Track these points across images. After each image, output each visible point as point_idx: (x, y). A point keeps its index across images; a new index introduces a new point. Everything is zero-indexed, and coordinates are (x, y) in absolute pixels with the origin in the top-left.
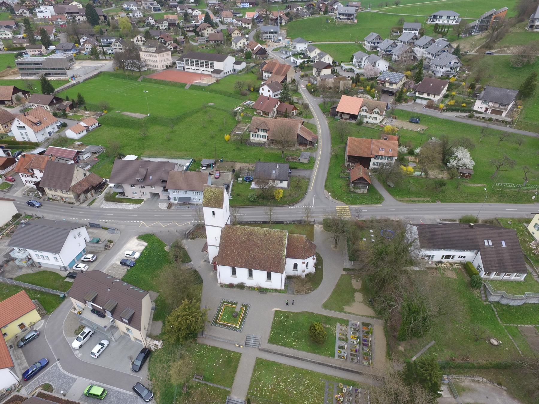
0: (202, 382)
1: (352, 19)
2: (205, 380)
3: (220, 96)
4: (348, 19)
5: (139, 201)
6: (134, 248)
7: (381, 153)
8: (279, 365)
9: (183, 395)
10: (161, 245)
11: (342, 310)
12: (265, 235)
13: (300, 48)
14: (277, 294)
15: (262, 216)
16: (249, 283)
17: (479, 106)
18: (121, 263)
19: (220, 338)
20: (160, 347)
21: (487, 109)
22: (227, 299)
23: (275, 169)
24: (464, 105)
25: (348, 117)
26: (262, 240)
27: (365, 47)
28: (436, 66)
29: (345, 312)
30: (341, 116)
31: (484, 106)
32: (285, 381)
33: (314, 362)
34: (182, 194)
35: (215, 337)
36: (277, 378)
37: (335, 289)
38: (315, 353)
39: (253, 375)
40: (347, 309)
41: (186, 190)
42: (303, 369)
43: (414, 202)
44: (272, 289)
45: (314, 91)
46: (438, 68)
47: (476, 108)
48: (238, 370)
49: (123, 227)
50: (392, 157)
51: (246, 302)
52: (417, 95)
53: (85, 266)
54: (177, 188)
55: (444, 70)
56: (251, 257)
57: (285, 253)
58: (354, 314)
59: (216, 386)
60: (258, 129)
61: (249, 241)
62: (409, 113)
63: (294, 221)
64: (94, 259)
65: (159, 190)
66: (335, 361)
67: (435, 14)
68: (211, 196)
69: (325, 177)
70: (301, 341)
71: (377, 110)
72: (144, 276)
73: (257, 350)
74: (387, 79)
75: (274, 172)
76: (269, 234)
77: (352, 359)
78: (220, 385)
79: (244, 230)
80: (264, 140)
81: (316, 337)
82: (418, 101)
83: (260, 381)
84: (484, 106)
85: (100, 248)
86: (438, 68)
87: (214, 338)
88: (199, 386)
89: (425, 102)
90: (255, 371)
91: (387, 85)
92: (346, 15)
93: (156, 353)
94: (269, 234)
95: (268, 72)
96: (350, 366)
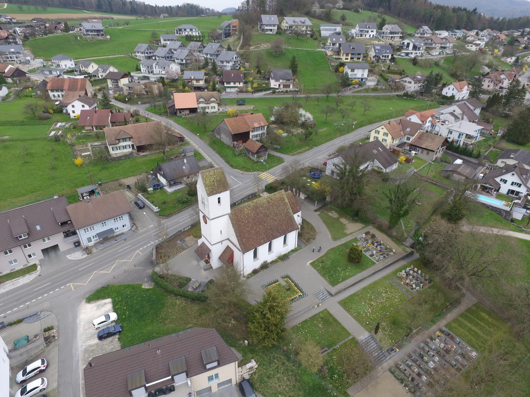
0: (329, 351)
1: (102, 35)
2: (329, 348)
3: (6, 127)
4: (98, 35)
5: (34, 267)
6: (99, 314)
7: (256, 125)
8: (355, 294)
9: (327, 375)
10: (135, 288)
11: (346, 235)
12: (269, 202)
13: (66, 65)
14: (297, 253)
15: (252, 187)
16: (270, 258)
17: (273, 84)
18: (101, 338)
19: (299, 312)
20: (257, 366)
21: (279, 85)
22: (266, 283)
23: (184, 164)
24: (264, 85)
25: (187, 112)
26: (268, 208)
27: (138, 58)
28: (222, 62)
29: (349, 234)
30: (180, 112)
31: (277, 83)
32: (371, 300)
33: (370, 276)
34: (99, 228)
35: (295, 314)
36: (365, 302)
37: (326, 225)
38: (364, 270)
39: (351, 314)
40: (347, 232)
41: (103, 221)
42: (370, 285)
43: (301, 152)
44: (289, 253)
45: (129, 100)
46: (225, 64)
47: (272, 86)
48: (338, 320)
49: (46, 305)
50: (264, 127)
51: (284, 274)
52: (225, 85)
53: (43, 381)
54: (89, 224)
55: (231, 64)
56: (267, 228)
57: (291, 211)
58: (354, 232)
59: (341, 343)
60: (119, 140)
61: (258, 215)
62: (234, 99)
63: (244, 198)
64: (45, 364)
65: (58, 239)
66: (379, 265)
67: (180, 27)
68: (213, 181)
69: (223, 161)
70: (349, 269)
71: (213, 99)
72: (149, 328)
73: (332, 298)
74: (193, 77)
75: (184, 167)
76: (271, 199)
77: (385, 257)
78: (343, 340)
79: (249, 206)
80: (129, 150)
81: (355, 258)
82: (228, 90)
83: (360, 313)
84: (277, 83)
85: (37, 347)
86: (225, 64)
87: (296, 315)
88: (332, 355)
89: (233, 90)
90: (348, 311)
91: (194, 82)
92: (94, 31)
93: (256, 377)
94: (271, 199)
95: (57, 91)
96: (389, 261)
